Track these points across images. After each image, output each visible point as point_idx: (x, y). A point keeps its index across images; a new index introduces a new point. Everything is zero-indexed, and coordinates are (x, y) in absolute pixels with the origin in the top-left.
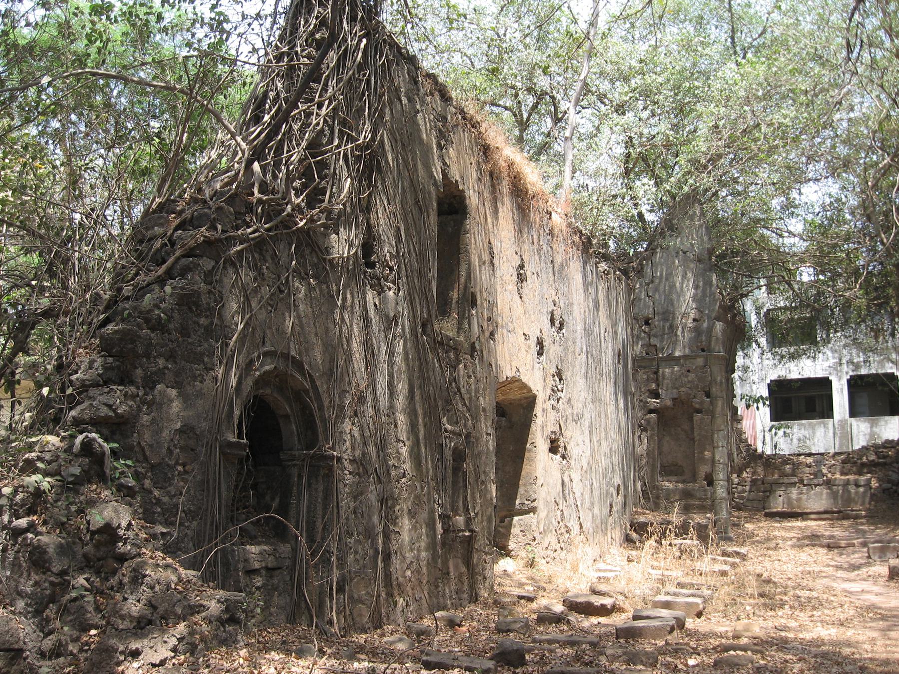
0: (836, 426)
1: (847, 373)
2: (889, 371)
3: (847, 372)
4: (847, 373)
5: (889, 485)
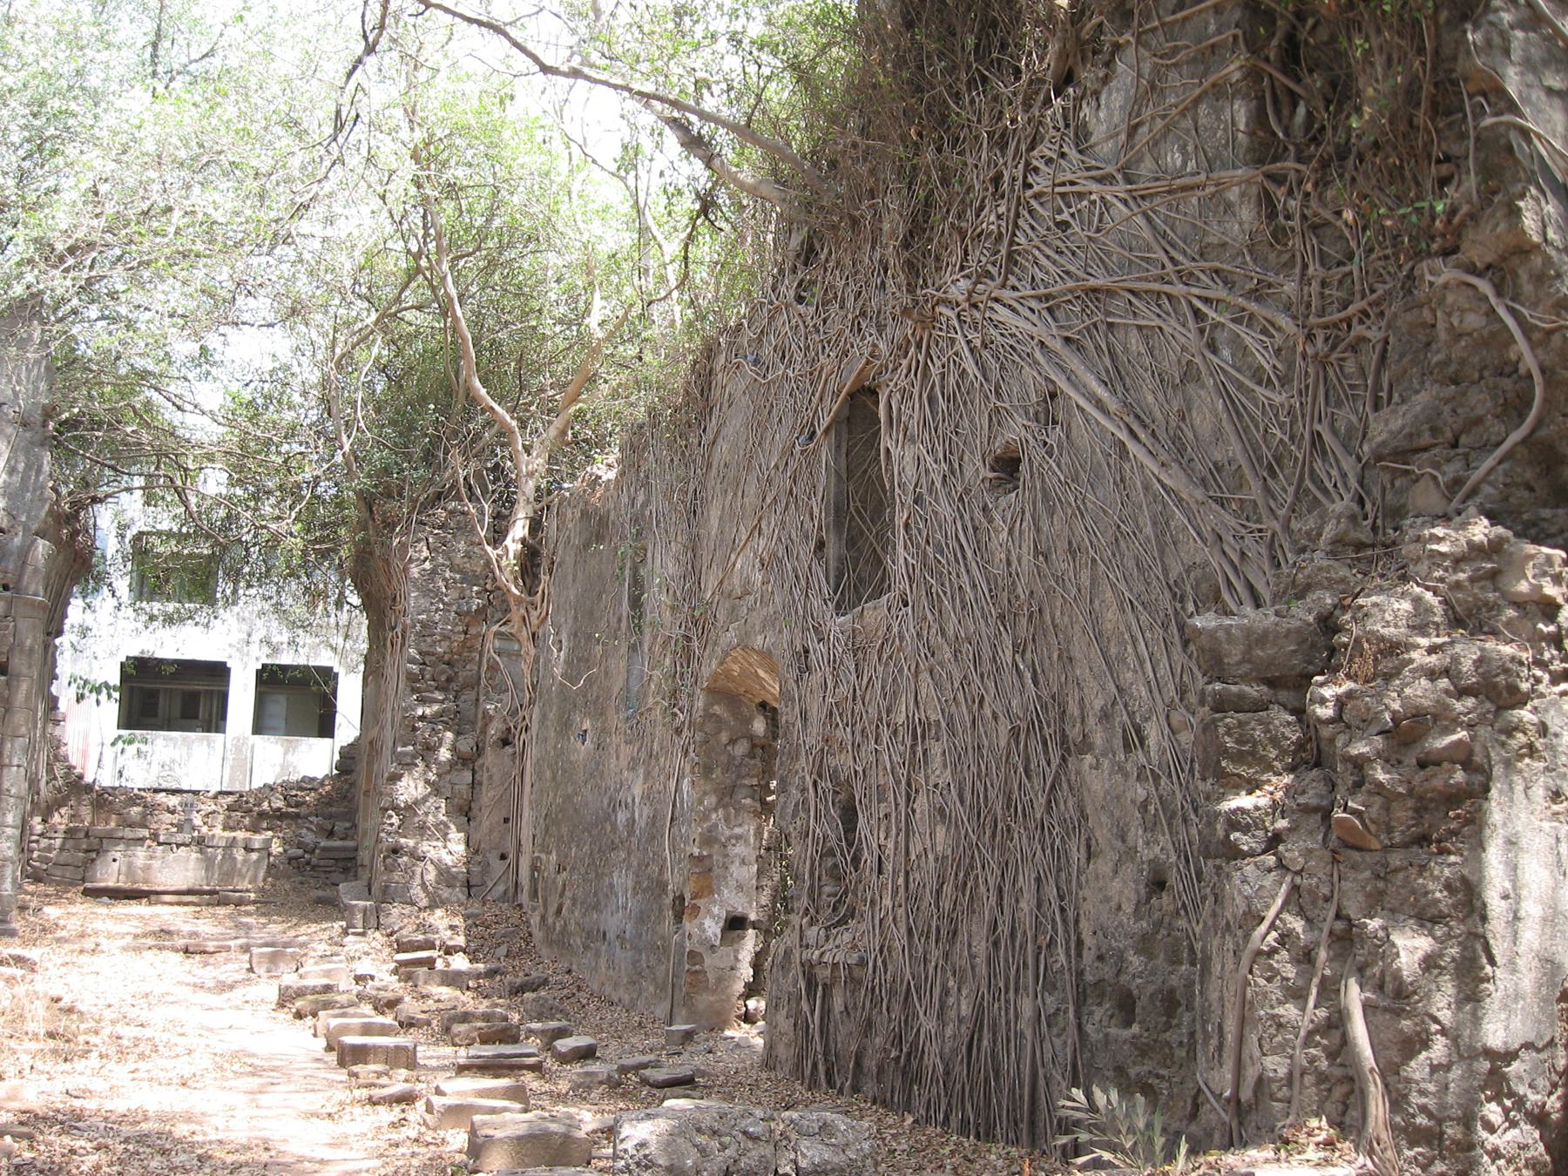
0: (229, 746)
3: (259, 657)
5: (300, 852)
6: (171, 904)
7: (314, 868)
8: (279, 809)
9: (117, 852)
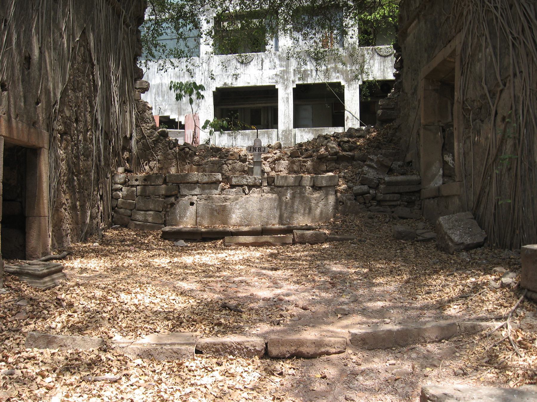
0: (280, 136)
1: (293, 82)
2: (335, 81)
3: (295, 80)
4: (293, 82)
5: (365, 188)
6: (246, 245)
7: (379, 203)
8: (336, 153)
9: (195, 195)
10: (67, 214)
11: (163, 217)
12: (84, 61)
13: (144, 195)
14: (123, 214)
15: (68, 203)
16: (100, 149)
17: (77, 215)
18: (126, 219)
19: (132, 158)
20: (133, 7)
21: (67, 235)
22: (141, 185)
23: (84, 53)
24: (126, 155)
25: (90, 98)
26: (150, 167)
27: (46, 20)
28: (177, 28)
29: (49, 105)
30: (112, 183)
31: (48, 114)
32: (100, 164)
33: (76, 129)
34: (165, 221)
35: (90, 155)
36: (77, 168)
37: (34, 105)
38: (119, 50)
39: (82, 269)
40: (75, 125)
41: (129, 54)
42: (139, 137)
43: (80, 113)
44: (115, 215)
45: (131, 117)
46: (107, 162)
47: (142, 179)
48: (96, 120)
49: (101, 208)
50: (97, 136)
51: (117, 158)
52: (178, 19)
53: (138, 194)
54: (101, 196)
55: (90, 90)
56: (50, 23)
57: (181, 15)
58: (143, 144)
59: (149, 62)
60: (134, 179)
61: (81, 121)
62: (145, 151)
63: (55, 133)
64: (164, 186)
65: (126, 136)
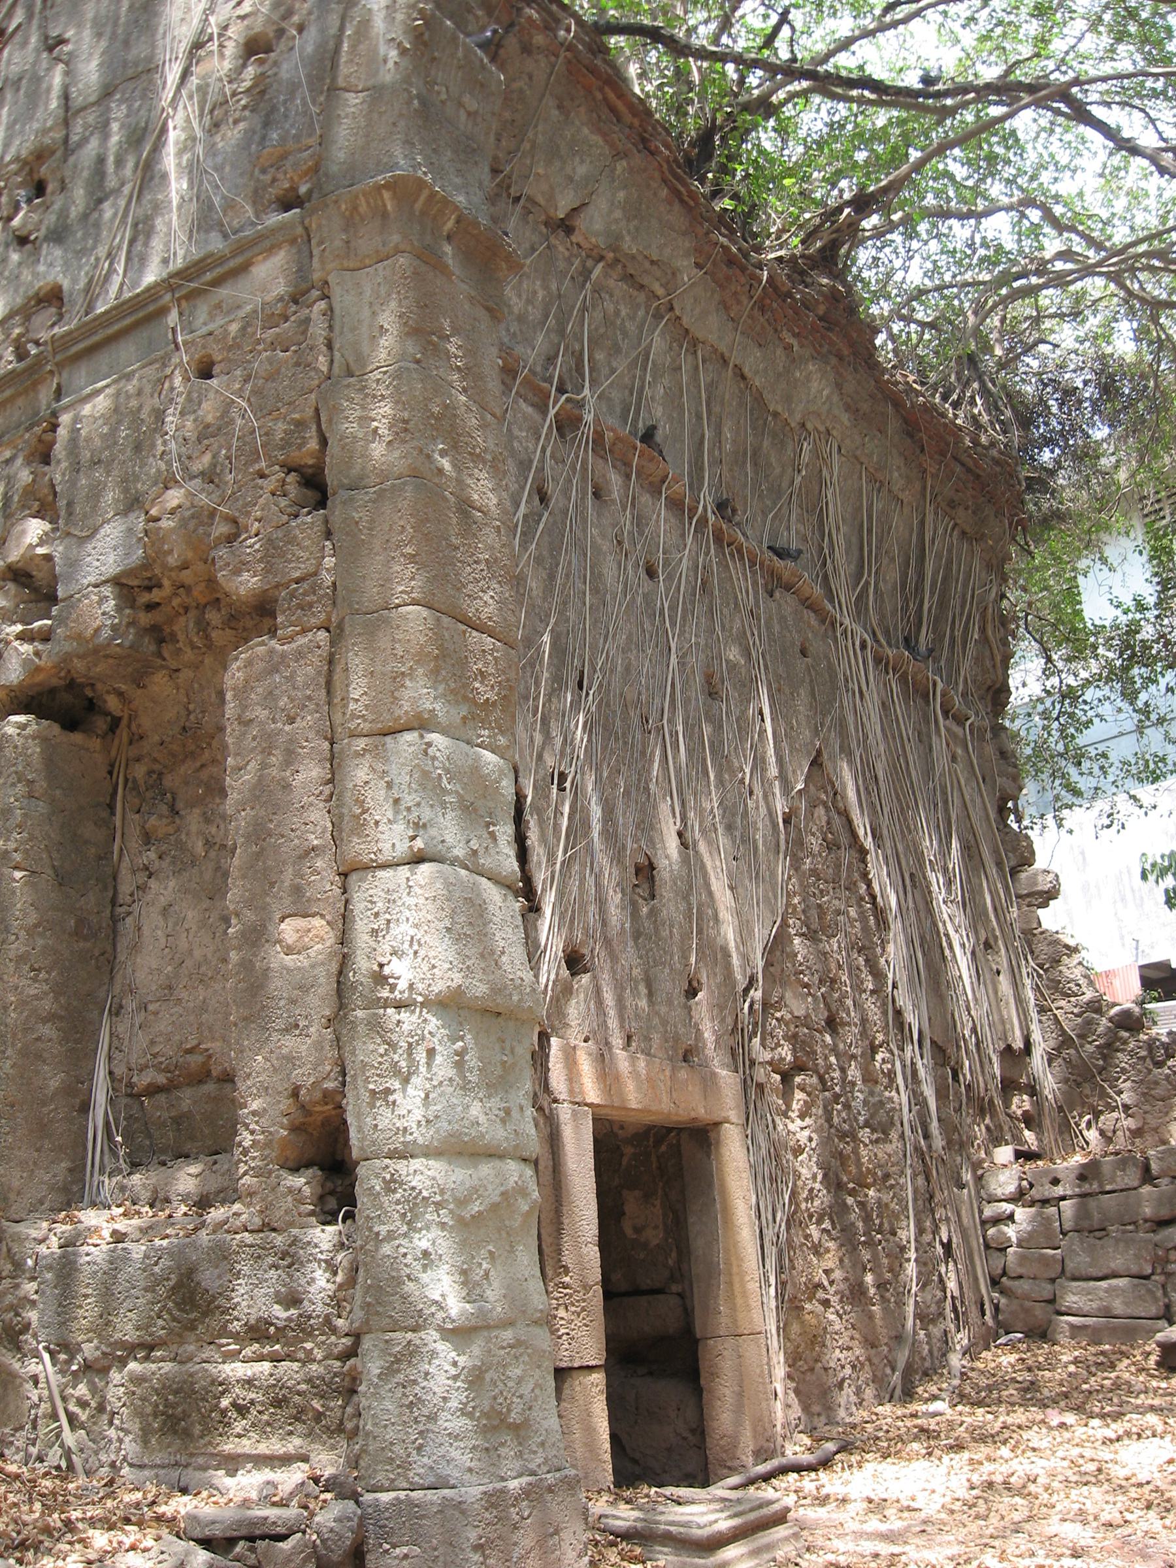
10: (833, 1317)
11: (1159, 1293)
12: (831, 846)
13: (1091, 1229)
14: (1027, 1297)
15: (832, 1283)
16: (925, 1099)
17: (871, 1316)
18: (1039, 1310)
19: (1040, 1112)
20: (967, 664)
21: (840, 1386)
22: (1071, 1197)
23: (828, 823)
24: (1021, 1103)
25: (868, 950)
26: (1102, 1133)
27: (690, 751)
28: (1130, 695)
29: (730, 995)
30: (980, 1199)
31: (730, 1020)
32: (930, 1147)
33: (834, 1050)
34: (1168, 1307)
35: (892, 1124)
36: (853, 1169)
37: (683, 1000)
38: (944, 793)
39: (870, 1501)
40: (828, 1039)
41: (978, 800)
42: (1052, 1043)
43: (840, 1001)
44: (1003, 1301)
45: (1016, 985)
46: (956, 1136)
47: (1073, 1176)
48: (898, 1013)
49: (952, 1285)
50: (908, 1062)
51: (987, 1121)
52: (1126, 669)
53: (1067, 1226)
54: (947, 1247)
55: (865, 928)
56: (704, 760)
57: (1134, 655)
58: (1068, 1062)
59: (1065, 813)
60: (1046, 1180)
61: (849, 1024)
62: (1079, 1085)
63: (760, 1074)
64: (1146, 1189)
65: (1009, 1047)
